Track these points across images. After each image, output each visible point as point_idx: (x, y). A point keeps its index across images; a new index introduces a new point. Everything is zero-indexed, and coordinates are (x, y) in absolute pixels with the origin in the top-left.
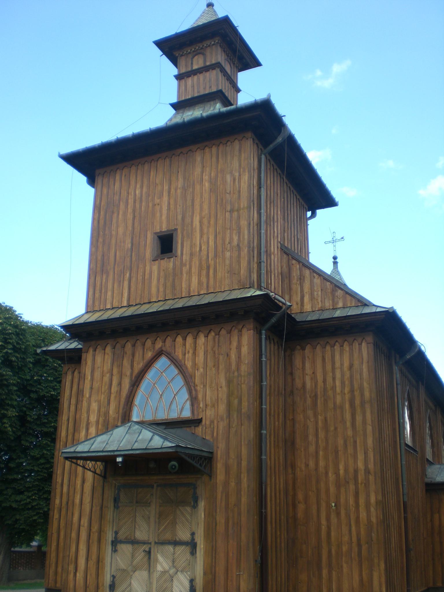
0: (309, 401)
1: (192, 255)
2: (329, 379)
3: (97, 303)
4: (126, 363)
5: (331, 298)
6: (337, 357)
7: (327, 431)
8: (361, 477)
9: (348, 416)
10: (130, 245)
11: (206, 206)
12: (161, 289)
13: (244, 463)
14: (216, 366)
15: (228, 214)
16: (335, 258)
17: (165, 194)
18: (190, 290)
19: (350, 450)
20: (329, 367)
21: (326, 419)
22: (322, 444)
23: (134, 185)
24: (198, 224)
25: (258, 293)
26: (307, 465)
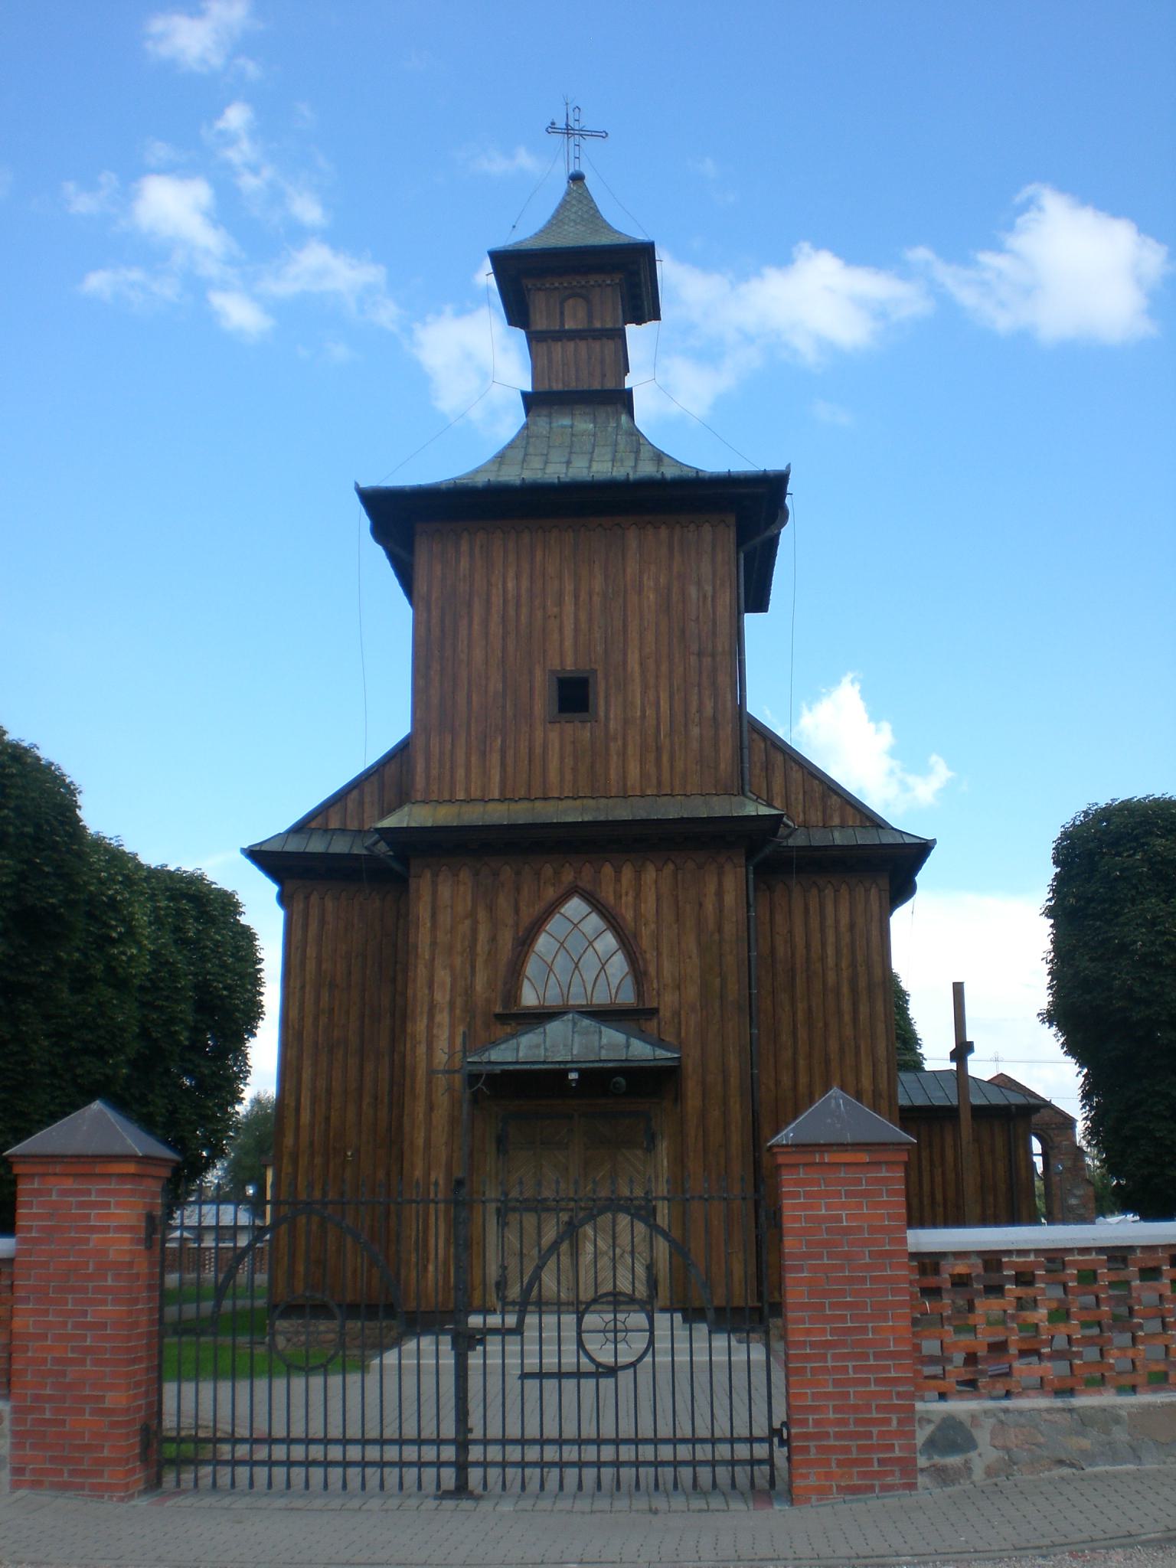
4: (503, 902)
5: (820, 808)
9: (846, 1005)
10: (500, 686)
12: (569, 777)
13: (734, 1081)
15: (693, 659)
17: (568, 599)
18: (625, 785)
20: (815, 923)
21: (810, 1009)
23: (500, 572)
24: (637, 668)
25: (764, 811)
26: (777, 1082)
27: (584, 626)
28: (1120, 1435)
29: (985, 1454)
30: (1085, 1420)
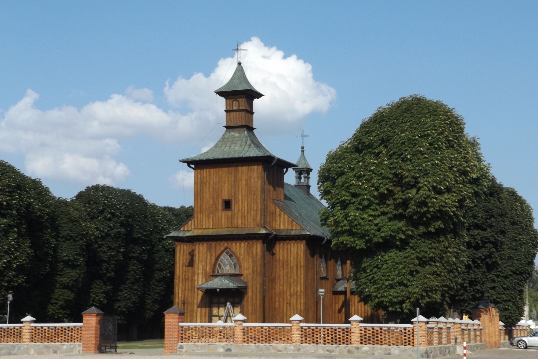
0: (281, 264)
1: (238, 211)
2: (289, 257)
3: (199, 225)
4: (213, 251)
6: (292, 249)
7: (287, 276)
8: (299, 293)
9: (295, 271)
11: (244, 191)
13: (258, 290)
14: (248, 255)
15: (252, 196)
16: (303, 148)
19: (295, 284)
22: (285, 281)
23: (211, 174)
25: (264, 232)
27: (230, 189)
28: (199, 348)
29: (184, 350)
30: (196, 346)
